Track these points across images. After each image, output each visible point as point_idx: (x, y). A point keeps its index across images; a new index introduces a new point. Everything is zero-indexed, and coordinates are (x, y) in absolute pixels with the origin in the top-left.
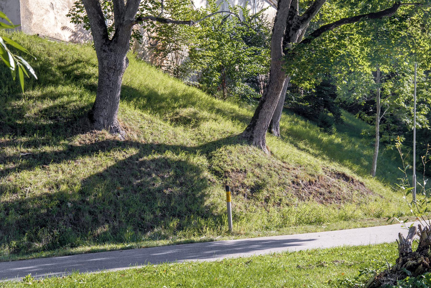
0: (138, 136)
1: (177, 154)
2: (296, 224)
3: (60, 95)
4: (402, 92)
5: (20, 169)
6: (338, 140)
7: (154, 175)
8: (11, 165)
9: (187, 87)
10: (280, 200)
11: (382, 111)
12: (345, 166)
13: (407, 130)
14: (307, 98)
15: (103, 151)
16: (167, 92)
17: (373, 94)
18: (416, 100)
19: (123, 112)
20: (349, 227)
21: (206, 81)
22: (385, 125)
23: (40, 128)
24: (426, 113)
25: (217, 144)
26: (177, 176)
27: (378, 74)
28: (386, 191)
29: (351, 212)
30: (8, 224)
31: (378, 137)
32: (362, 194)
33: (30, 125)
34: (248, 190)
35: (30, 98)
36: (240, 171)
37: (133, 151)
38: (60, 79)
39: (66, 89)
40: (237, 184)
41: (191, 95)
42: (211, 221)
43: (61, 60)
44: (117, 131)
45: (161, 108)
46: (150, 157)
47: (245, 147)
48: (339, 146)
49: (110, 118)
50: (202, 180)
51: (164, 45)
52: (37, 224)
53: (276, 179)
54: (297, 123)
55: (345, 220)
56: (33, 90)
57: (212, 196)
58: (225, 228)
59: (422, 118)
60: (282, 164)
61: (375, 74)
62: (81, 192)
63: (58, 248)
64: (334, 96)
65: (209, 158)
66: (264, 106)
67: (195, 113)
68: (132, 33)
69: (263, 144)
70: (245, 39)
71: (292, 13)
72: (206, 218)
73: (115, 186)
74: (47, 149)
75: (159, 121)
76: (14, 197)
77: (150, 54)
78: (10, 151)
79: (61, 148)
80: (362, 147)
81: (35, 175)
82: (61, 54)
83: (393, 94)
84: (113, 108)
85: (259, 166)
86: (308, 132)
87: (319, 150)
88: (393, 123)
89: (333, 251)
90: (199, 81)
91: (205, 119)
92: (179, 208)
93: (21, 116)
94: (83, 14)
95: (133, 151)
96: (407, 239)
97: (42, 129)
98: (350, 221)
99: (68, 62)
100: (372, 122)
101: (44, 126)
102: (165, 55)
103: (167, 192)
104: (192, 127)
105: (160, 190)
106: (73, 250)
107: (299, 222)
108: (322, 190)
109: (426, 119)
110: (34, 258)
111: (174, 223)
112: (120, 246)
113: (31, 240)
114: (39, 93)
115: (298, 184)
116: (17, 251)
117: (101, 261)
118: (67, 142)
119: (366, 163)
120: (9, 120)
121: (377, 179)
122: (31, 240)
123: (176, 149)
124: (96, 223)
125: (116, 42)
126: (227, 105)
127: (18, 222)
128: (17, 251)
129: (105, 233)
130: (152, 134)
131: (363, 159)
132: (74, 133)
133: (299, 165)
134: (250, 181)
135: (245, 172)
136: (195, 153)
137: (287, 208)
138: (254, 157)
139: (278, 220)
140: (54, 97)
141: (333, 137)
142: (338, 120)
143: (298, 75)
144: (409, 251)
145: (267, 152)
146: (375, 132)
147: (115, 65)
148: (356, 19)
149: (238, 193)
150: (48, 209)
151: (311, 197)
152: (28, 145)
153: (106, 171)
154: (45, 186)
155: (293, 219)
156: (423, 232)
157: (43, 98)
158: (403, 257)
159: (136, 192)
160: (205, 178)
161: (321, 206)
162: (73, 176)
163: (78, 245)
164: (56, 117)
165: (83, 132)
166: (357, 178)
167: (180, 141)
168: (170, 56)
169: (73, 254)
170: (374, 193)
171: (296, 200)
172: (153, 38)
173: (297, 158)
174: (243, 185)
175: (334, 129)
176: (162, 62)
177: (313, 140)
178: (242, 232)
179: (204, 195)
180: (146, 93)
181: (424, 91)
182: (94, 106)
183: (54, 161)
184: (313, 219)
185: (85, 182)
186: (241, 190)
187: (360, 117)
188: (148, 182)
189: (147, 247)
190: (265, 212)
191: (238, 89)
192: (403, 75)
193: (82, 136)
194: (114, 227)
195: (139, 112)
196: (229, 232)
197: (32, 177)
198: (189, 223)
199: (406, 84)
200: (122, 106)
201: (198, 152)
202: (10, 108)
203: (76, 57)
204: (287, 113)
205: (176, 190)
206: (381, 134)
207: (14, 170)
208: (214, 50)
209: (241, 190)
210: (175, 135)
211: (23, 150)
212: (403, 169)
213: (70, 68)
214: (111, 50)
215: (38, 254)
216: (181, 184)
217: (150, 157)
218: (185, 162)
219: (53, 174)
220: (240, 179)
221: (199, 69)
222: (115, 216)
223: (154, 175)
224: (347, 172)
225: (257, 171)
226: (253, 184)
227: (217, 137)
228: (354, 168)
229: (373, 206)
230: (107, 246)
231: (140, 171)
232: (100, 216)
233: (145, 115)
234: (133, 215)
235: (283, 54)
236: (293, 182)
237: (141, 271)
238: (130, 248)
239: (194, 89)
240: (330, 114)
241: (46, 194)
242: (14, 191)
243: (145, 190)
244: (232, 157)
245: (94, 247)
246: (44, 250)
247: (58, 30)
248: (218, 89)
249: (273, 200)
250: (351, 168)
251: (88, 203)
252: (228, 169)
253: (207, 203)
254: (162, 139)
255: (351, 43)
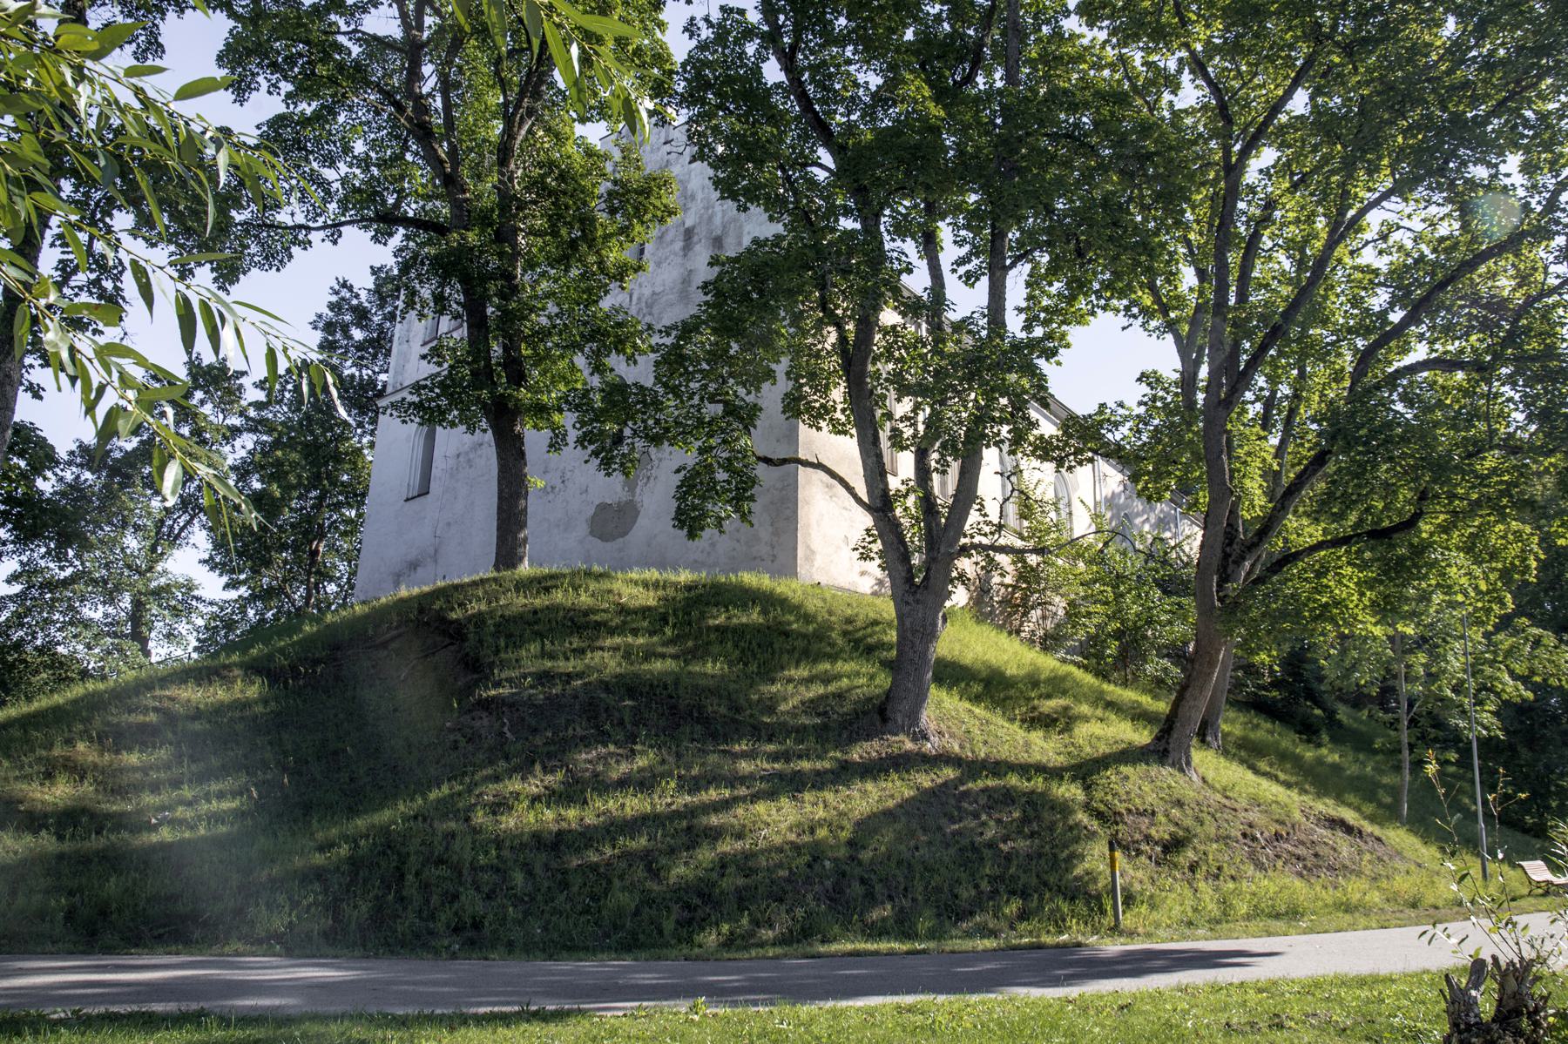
0: (962, 747)
1: (1029, 780)
2: (1248, 917)
3: (838, 677)
4: (1444, 671)
5: (755, 798)
6: (1335, 758)
7: (984, 817)
8: (743, 791)
9: (1058, 664)
10: (1219, 868)
11: (1411, 705)
12: (1349, 805)
13: (1461, 741)
14: (1276, 684)
15: (897, 771)
16: (1022, 672)
17: (1390, 674)
18: (1472, 685)
19: (939, 704)
20: (1353, 927)
21: (1095, 656)
22: (1417, 731)
23: (797, 731)
24: (1493, 708)
25: (1103, 762)
26: (1025, 820)
27: (1398, 639)
28: (1428, 853)
29: (1358, 896)
30: (722, 893)
31: (1406, 752)
32: (1380, 859)
33: (784, 724)
34: (1158, 849)
35: (790, 680)
36: (1143, 813)
37: (949, 773)
38: (842, 650)
39: (848, 667)
40: (1137, 836)
41: (1064, 678)
42: (1081, 907)
43: (849, 621)
44: (926, 738)
45: (1007, 698)
46: (980, 784)
47: (1154, 770)
48: (1335, 768)
49: (914, 716)
50: (1071, 828)
51: (1025, 598)
52: (768, 897)
53: (1211, 829)
54: (1257, 726)
55: (1346, 911)
56: (797, 667)
57: (1088, 858)
58: (1108, 921)
59: (1486, 718)
60: (1224, 801)
61: (1391, 639)
62: (851, 843)
63: (799, 941)
64: (1321, 679)
65: (1087, 788)
66: (1188, 695)
67: (1066, 709)
68: (954, 574)
69: (1188, 763)
70: (1160, 584)
71: (1230, 535)
72: (1073, 899)
73: (912, 834)
74: (805, 765)
75: (1000, 721)
76: (739, 845)
77: (1002, 613)
78: (745, 766)
79: (827, 765)
80: (1381, 772)
81: (778, 810)
82: (849, 611)
83: (1429, 675)
84: (920, 699)
85: (1179, 804)
86: (1277, 743)
87: (1297, 774)
88: (1433, 726)
89: (1312, 987)
90: (1081, 654)
91: (1086, 719)
92: (1024, 879)
93: (771, 710)
94: (878, 546)
95: (949, 773)
96: (1467, 989)
97: (801, 732)
98: (1357, 915)
99: (859, 624)
100: (1394, 724)
101: (805, 727)
102: (1025, 614)
103: (1005, 847)
104: (1060, 733)
105: (991, 845)
106: (822, 949)
107: (1255, 914)
108: (1301, 851)
109: (1494, 720)
110: (750, 959)
111: (1011, 909)
112: (905, 947)
113: (757, 923)
114: (806, 674)
115: (1254, 839)
116: (729, 943)
117: (857, 976)
118: (838, 755)
119: (1388, 800)
120: (751, 716)
121: (1410, 830)
122: (757, 923)
123: (1025, 770)
124: (871, 899)
125: (926, 588)
126: (1129, 695)
127: (738, 890)
128: (729, 943)
129: (884, 920)
130: (985, 743)
131: (1381, 792)
132: (853, 739)
133: (1255, 802)
134: (1162, 831)
135: (1153, 813)
136: (1062, 778)
137: (1231, 885)
138: (1170, 787)
139: (1213, 908)
140: (827, 679)
141: (1324, 751)
142: (1331, 721)
143: (1245, 640)
144: (1473, 1021)
145: (1195, 778)
146: (1399, 742)
147: (924, 626)
148: (1346, 540)
149: (1139, 853)
150: (790, 869)
151: (1280, 863)
152: (774, 757)
153: (900, 806)
154: (790, 829)
155: (1243, 909)
156: (1504, 974)
157: (810, 680)
158: (1460, 1032)
159: (948, 845)
160: (1077, 825)
161: (1298, 883)
162: (841, 814)
163: (835, 939)
164: (826, 713)
165: (868, 738)
166: (1368, 827)
167: (1036, 757)
168: (1035, 614)
169: (819, 956)
170: (1403, 858)
171: (1250, 870)
172: (1007, 586)
173: (1251, 790)
174: (1148, 838)
175: (1325, 738)
176: (1021, 624)
177: (1284, 757)
178: (1140, 930)
179: (1073, 856)
180: (984, 675)
181: (1486, 667)
182: (888, 695)
183: (813, 786)
184: (1283, 909)
185: (859, 824)
186: (1144, 847)
187: (1370, 716)
188: (972, 830)
189: (953, 952)
190: (1188, 893)
191: (1149, 668)
192: (1444, 640)
193: (866, 745)
194: (902, 909)
195: (967, 705)
196: (1115, 930)
197: (774, 812)
198: (1041, 907)
199: (1450, 658)
200: (935, 694)
201: (1067, 776)
202: (756, 697)
203: (872, 615)
204: (1240, 710)
205: (1022, 844)
206: (1411, 747)
207: (743, 799)
208: (1106, 603)
209: (1144, 847)
210: (1027, 744)
211: (766, 766)
212: (1448, 824)
213: (861, 633)
214: (918, 602)
215: (761, 951)
216: (1032, 835)
217: (980, 784)
218: (1043, 794)
219: (808, 808)
220: (1143, 827)
221: (1081, 635)
222: (906, 889)
223: (984, 817)
224: (1349, 815)
225: (1175, 812)
226: (1167, 837)
227: (1103, 749)
228: (1364, 809)
229: (1403, 884)
230: (884, 946)
231: (959, 808)
232: (878, 887)
233: (977, 711)
234: (938, 889)
235: (1218, 604)
236: (1244, 835)
237: (911, 1009)
238: (924, 952)
239: (1073, 669)
240: (1318, 712)
241: (792, 843)
242: (740, 836)
243: (965, 842)
244: (1129, 786)
245: (862, 946)
246: (774, 944)
247: (855, 577)
248: (1116, 669)
249: (1204, 868)
250: (1358, 809)
251: (860, 864)
252: (1121, 807)
253: (1078, 871)
254: (1004, 752)
255: (1340, 582)
